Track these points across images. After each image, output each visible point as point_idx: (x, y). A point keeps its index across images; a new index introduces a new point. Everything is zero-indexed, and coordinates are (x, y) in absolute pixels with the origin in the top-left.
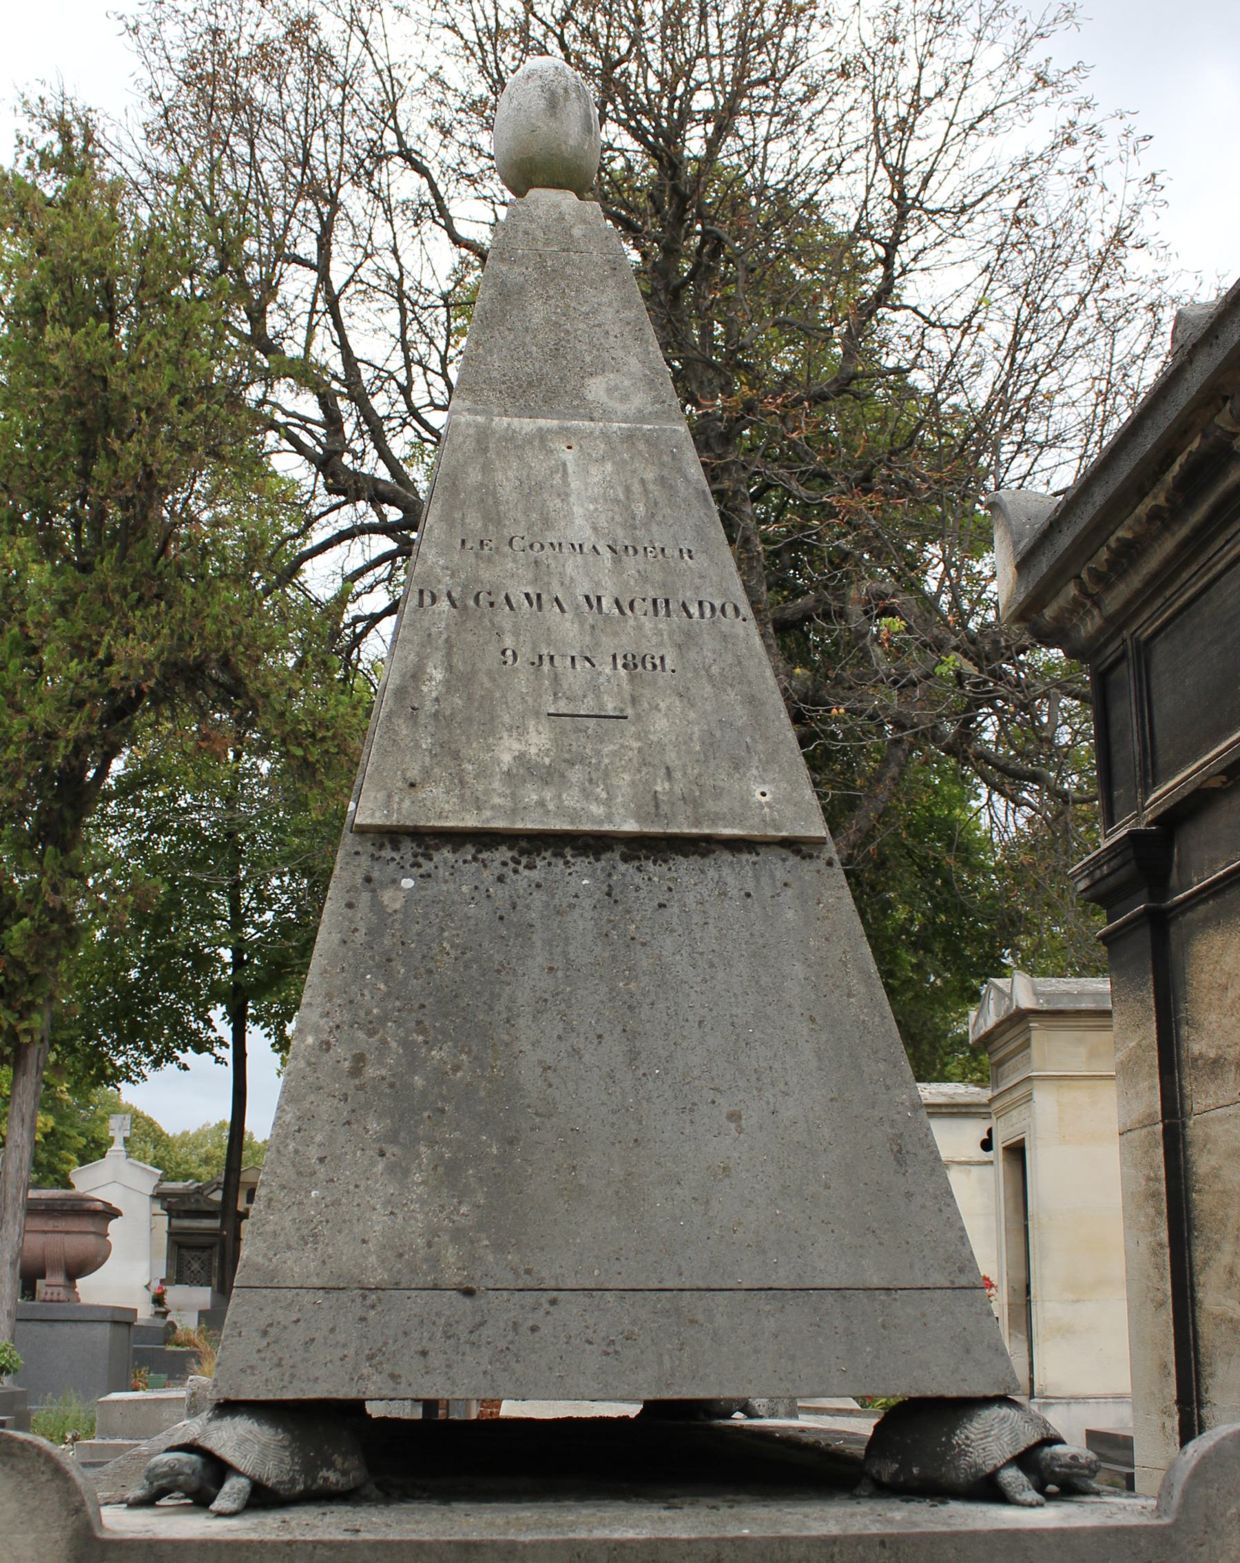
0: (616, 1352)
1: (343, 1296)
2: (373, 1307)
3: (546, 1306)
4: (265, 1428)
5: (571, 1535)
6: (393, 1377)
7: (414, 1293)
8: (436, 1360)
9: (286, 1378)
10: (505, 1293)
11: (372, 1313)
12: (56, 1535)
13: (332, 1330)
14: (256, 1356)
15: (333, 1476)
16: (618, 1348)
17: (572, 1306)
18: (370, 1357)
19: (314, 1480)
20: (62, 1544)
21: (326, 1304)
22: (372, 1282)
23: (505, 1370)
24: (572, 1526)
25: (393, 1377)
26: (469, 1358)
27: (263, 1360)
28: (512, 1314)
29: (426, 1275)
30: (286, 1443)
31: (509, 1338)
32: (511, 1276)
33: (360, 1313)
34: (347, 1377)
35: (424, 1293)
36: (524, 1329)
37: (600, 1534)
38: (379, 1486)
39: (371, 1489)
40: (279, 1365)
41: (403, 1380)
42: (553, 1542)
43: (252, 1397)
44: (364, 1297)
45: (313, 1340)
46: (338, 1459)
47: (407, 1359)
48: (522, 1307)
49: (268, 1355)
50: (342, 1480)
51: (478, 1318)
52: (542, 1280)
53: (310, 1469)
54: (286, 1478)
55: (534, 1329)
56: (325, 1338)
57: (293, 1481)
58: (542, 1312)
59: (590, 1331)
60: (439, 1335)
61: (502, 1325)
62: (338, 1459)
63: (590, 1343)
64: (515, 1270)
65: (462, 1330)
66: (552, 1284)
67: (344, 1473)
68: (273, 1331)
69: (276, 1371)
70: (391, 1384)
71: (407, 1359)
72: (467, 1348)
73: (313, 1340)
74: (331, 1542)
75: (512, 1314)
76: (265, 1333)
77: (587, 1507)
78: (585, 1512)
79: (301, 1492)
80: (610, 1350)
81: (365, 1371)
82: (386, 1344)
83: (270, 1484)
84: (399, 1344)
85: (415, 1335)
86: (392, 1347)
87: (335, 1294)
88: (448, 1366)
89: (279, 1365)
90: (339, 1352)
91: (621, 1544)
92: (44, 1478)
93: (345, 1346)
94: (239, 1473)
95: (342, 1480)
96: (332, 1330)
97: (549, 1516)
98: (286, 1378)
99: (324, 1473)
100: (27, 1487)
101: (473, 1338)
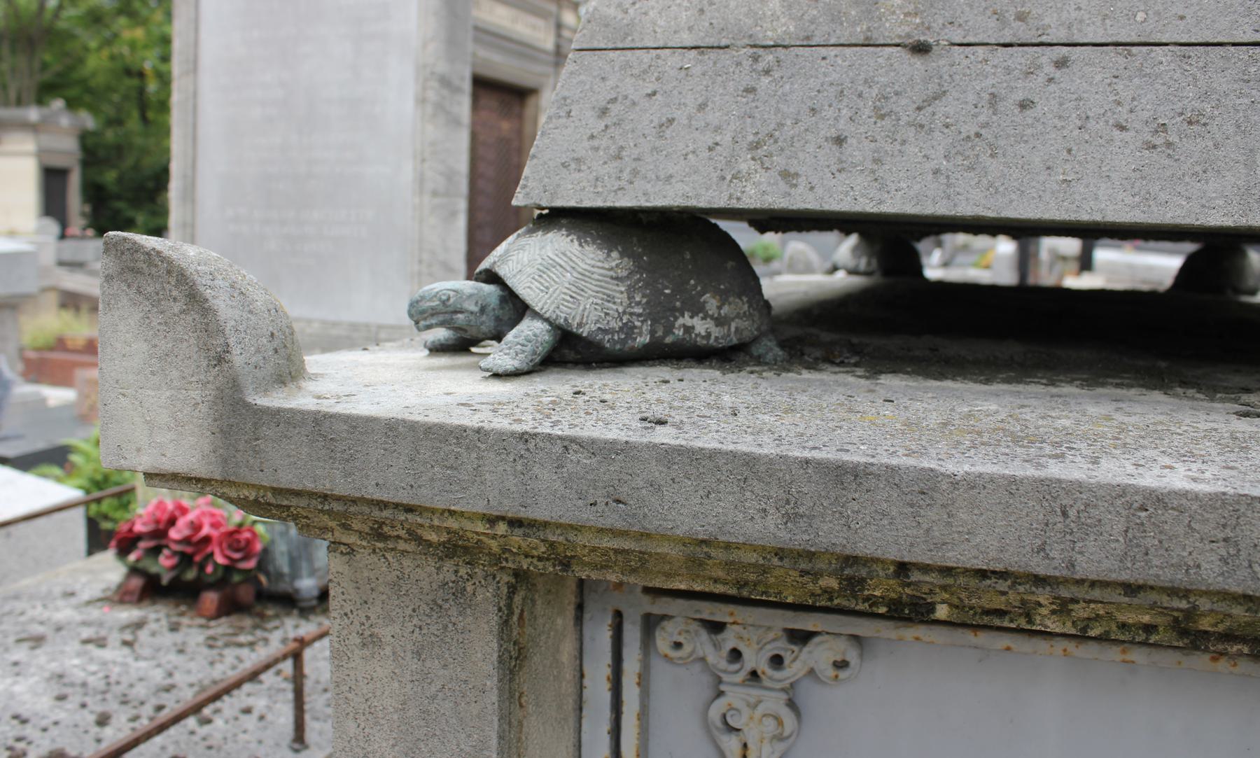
0: (1169, 145)
1: (724, 56)
2: (767, 72)
3: (1050, 69)
5: (1054, 470)
6: (786, 175)
7: (833, 52)
8: (856, 151)
9: (625, 176)
10: (980, 49)
11: (766, 80)
12: (196, 394)
13: (702, 107)
14: (586, 144)
15: (701, 326)
16: (1173, 138)
17: (1092, 75)
18: (755, 146)
19: (669, 330)
20: (204, 408)
21: (697, 70)
22: (770, 37)
23: (971, 168)
24: (1062, 448)
25: (786, 175)
26: (911, 149)
27: (597, 149)
28: (990, 81)
29: (854, 24)
31: (982, 118)
32: (992, 23)
33: (747, 81)
34: (715, 176)
35: (848, 51)
36: (1009, 105)
37: (1115, 470)
40: (618, 157)
41: (802, 181)
42: (1013, 480)
43: (572, 203)
44: (756, 59)
45: (671, 121)
46: (711, 303)
47: (811, 148)
48: (1008, 71)
49: (605, 142)
50: (716, 332)
51: (933, 88)
52: (1044, 29)
53: (660, 312)
54: (616, 325)
55: (1024, 105)
56: (690, 118)
57: (628, 329)
58: (1041, 79)
59: (1123, 111)
60: (867, 112)
61: (971, 98)
62: (711, 303)
63: (1122, 128)
64: (999, 16)
65: (904, 107)
66: (1062, 36)
67: (720, 321)
68: (615, 109)
69: (612, 167)
70: (783, 186)
71: (811, 148)
72: (911, 133)
73: (671, 121)
74: (593, 441)
75: (990, 81)
76: (604, 112)
77: (1097, 400)
78: (1093, 410)
80: (1159, 141)
81: (743, 167)
82: (780, 125)
83: (584, 332)
84: (801, 127)
85: (829, 113)
86: (788, 131)
87: (713, 54)
88: (876, 161)
89: (618, 157)
90: (709, 139)
91: (1159, 499)
92: (177, 307)
93: (717, 129)
94: (537, 315)
95: (716, 332)
96: (702, 107)
97: (1027, 415)
98: (625, 176)
99: (686, 320)
100: (156, 320)
101: (922, 118)
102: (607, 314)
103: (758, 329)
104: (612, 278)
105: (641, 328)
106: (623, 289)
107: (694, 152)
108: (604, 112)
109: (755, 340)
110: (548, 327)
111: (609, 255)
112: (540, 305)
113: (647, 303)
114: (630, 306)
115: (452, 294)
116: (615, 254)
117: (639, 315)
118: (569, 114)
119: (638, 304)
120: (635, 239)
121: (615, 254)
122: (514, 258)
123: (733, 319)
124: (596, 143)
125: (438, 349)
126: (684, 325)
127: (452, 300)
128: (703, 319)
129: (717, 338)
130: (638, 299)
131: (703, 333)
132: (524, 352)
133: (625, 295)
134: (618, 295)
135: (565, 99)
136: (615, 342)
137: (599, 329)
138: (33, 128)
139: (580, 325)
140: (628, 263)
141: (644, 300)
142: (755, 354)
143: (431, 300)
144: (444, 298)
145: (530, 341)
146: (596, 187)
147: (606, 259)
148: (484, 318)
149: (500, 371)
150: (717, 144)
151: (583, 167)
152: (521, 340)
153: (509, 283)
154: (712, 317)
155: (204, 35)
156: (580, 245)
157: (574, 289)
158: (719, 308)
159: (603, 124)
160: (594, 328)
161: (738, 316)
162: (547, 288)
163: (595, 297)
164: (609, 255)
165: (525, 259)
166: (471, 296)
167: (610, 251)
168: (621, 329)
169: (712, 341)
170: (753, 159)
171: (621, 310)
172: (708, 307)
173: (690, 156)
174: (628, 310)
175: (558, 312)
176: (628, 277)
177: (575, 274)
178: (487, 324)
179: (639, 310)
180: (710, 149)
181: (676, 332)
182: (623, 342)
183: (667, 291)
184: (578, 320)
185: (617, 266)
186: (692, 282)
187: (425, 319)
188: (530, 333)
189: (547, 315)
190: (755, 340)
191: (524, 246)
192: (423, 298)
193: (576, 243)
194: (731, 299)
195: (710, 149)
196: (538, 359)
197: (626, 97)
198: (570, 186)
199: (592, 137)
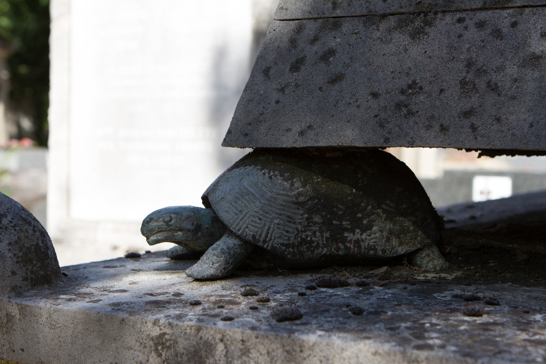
112: (234, 226)
175: (247, 230)
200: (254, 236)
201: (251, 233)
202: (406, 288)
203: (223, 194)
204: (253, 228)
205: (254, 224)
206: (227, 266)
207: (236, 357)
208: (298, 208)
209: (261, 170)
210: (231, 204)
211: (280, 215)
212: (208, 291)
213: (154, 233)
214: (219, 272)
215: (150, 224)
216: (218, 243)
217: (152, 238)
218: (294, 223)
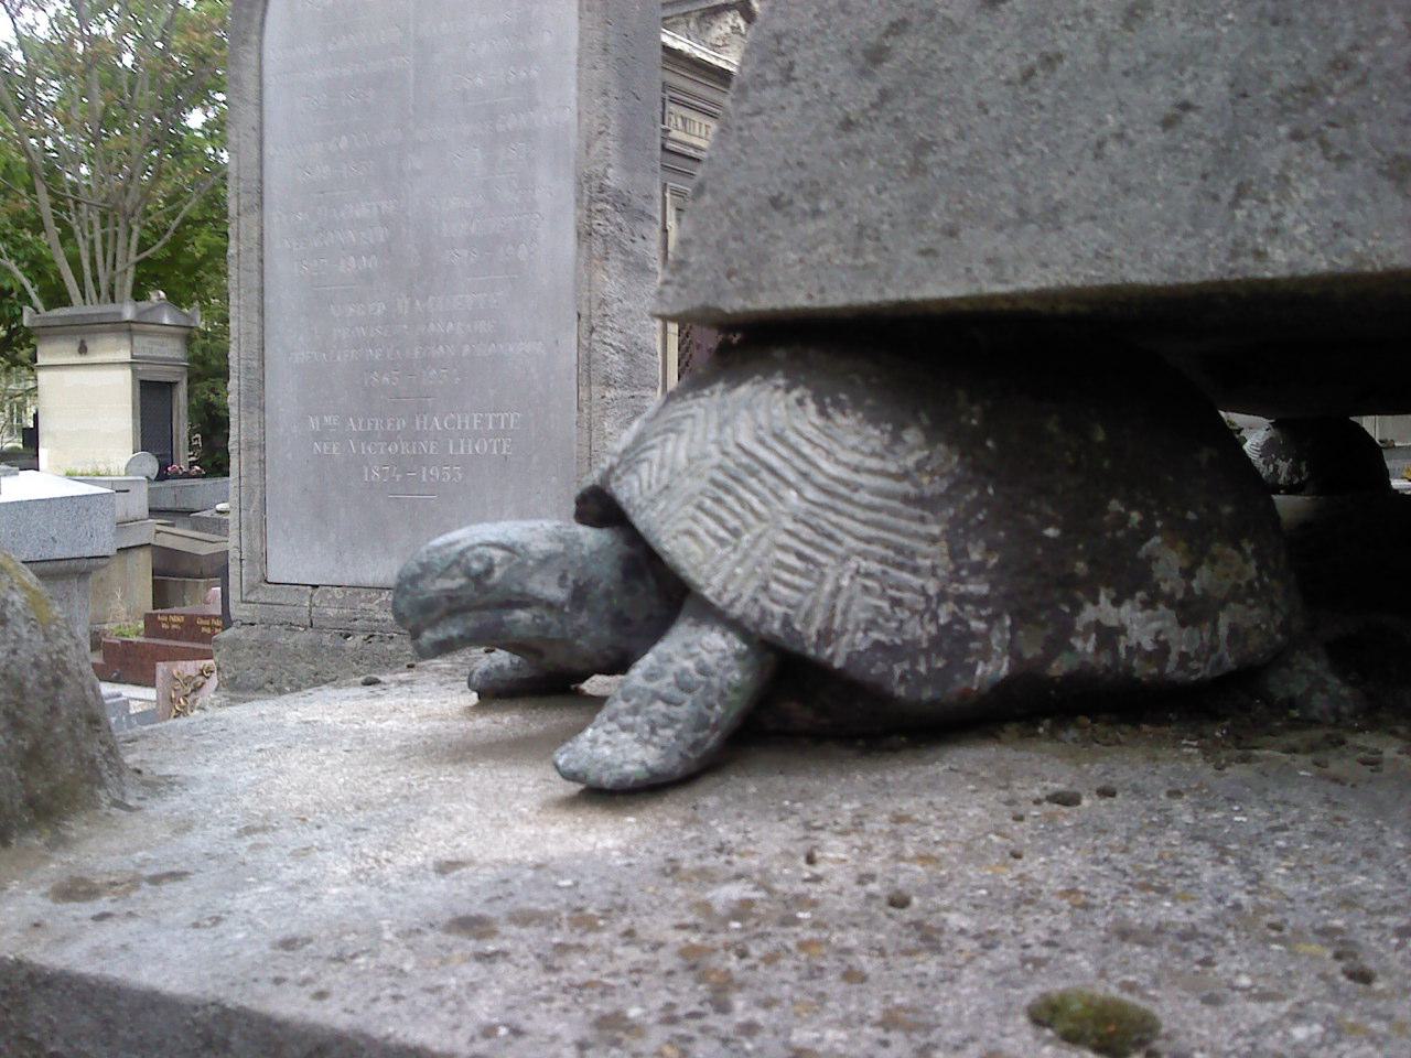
4: (845, 422)
15: (1141, 626)
19: (1059, 643)
30: (933, 486)
38: (1346, 656)
39: (1313, 679)
45: (1051, 61)
46: (1166, 560)
50: (1182, 641)
53: (1036, 592)
54: (920, 631)
56: (1105, 45)
57: (955, 643)
67: (1191, 611)
79: (1002, 689)
90: (1160, 96)
94: (711, 614)
95: (1182, 641)
99: (1102, 610)
102: (896, 602)
103: (1284, 628)
104: (906, 499)
105: (985, 637)
106: (936, 530)
107: (1120, 136)
108: (877, 56)
109: (1279, 658)
110: (738, 645)
111: (896, 438)
112: (716, 581)
113: (1001, 567)
114: (955, 577)
115: (498, 555)
116: (912, 436)
117: (981, 601)
118: (787, 76)
119: (978, 569)
120: (961, 394)
121: (912, 436)
122: (655, 454)
123: (1223, 604)
124: (856, 139)
125: (493, 693)
126: (1098, 626)
127: (498, 574)
128: (1148, 604)
129: (1184, 658)
130: (976, 557)
131: (1148, 646)
132: (671, 721)
133: (943, 547)
134: (923, 547)
135: (778, 37)
136: (923, 681)
137: (878, 645)
138: (127, 329)
139: (826, 636)
140: (948, 459)
141: (993, 561)
142: (1281, 695)
143: (445, 573)
144: (476, 566)
145: (686, 688)
146: (857, 253)
147: (889, 449)
148: (584, 618)
149: (607, 779)
150: (1186, 106)
151: (824, 205)
152: (664, 685)
153: (640, 521)
154: (1170, 601)
155: (269, 150)
156: (822, 412)
157: (806, 533)
158: (1188, 573)
159: (874, 89)
160: (861, 642)
161: (1235, 595)
162: (735, 533)
163: (864, 555)
164: (896, 438)
165: (682, 455)
166: (546, 560)
167: (900, 426)
168: (935, 642)
169: (1171, 667)
170: (1296, 136)
171: (932, 587)
172: (1159, 570)
173: (1112, 147)
174: (954, 588)
175: (765, 601)
176: (947, 498)
177: (811, 493)
178: (591, 631)
179: (979, 588)
180: (1168, 123)
181: (1078, 643)
182: (937, 677)
183: (1051, 532)
184: (818, 622)
185: (919, 466)
186: (1115, 505)
187: (433, 625)
188: (695, 656)
189: (736, 611)
190: (1279, 658)
191: (678, 421)
192: (426, 568)
193: (811, 407)
194: (1216, 548)
195: (1168, 123)
196: (712, 740)
197: (931, 14)
198: (793, 256)
199: (848, 125)
200: (787, 621)
201: (778, 610)
202: (577, 762)
203: (665, 473)
204: (785, 591)
205: (786, 576)
206: (700, 735)
207: (465, 998)
208: (922, 520)
209: (788, 390)
210: (700, 507)
211: (869, 541)
212: (464, 810)
213: (436, 615)
214: (675, 759)
215: (421, 585)
216: (661, 647)
217: (428, 636)
218: (915, 571)
